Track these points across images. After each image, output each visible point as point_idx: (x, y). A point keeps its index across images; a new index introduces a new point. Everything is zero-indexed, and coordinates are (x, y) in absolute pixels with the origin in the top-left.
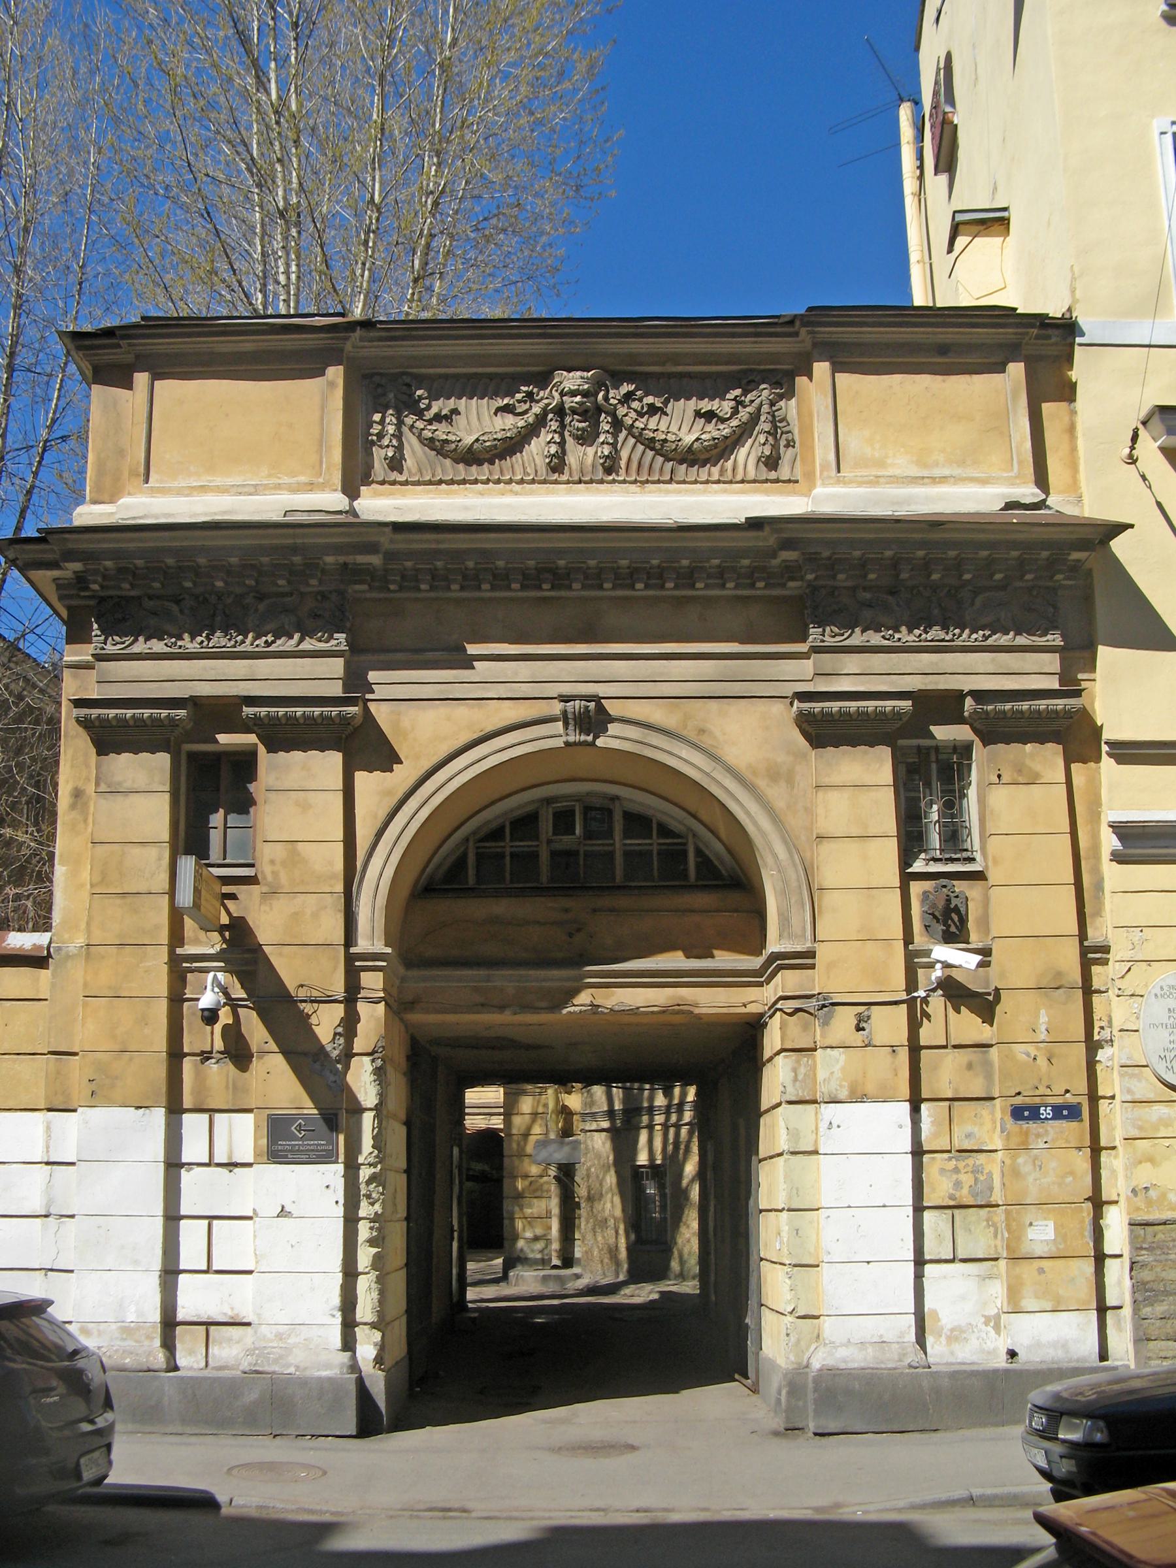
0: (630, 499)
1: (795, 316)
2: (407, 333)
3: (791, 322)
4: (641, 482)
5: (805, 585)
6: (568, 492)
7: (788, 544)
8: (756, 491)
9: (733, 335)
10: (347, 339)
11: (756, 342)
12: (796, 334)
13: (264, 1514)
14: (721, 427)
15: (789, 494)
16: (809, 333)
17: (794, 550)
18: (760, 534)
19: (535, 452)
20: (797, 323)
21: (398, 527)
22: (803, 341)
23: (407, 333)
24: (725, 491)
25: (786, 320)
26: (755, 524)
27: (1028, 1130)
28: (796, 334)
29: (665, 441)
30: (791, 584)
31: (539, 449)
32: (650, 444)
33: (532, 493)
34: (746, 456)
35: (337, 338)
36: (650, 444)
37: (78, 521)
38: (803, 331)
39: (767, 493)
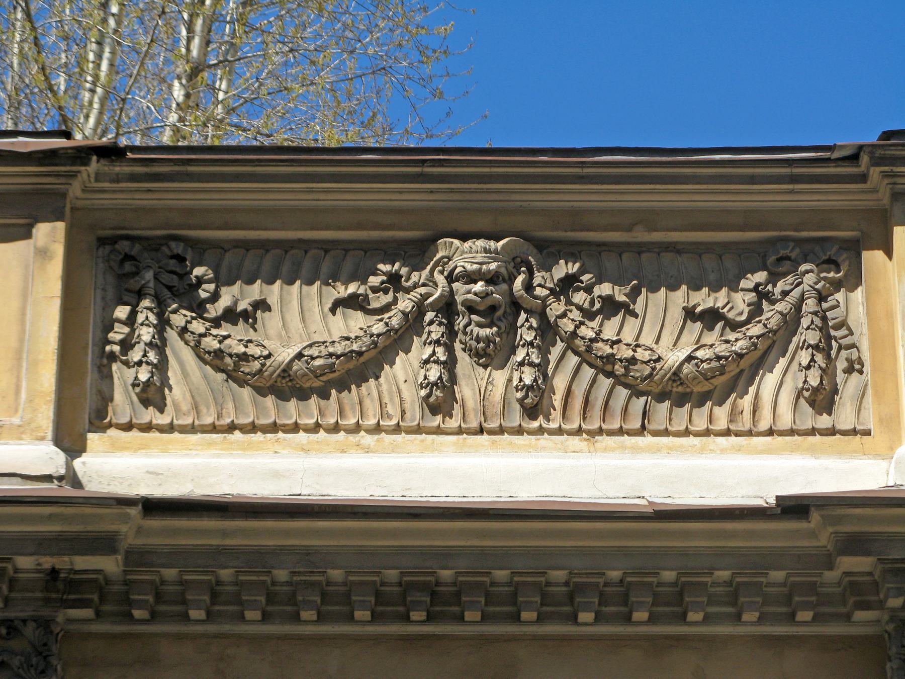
0: (570, 461)
1: (861, 147)
7: (854, 544)
8: (794, 450)
9: (752, 180)
10: (74, 175)
11: (792, 192)
12: (863, 178)
16: (886, 175)
17: (867, 553)
19: (401, 378)
20: (865, 159)
22: (875, 191)
24: (739, 449)
26: (794, 508)
28: (863, 178)
29: (633, 361)
32: (605, 366)
35: (57, 175)
36: (605, 366)
38: (875, 173)
39: (813, 451)
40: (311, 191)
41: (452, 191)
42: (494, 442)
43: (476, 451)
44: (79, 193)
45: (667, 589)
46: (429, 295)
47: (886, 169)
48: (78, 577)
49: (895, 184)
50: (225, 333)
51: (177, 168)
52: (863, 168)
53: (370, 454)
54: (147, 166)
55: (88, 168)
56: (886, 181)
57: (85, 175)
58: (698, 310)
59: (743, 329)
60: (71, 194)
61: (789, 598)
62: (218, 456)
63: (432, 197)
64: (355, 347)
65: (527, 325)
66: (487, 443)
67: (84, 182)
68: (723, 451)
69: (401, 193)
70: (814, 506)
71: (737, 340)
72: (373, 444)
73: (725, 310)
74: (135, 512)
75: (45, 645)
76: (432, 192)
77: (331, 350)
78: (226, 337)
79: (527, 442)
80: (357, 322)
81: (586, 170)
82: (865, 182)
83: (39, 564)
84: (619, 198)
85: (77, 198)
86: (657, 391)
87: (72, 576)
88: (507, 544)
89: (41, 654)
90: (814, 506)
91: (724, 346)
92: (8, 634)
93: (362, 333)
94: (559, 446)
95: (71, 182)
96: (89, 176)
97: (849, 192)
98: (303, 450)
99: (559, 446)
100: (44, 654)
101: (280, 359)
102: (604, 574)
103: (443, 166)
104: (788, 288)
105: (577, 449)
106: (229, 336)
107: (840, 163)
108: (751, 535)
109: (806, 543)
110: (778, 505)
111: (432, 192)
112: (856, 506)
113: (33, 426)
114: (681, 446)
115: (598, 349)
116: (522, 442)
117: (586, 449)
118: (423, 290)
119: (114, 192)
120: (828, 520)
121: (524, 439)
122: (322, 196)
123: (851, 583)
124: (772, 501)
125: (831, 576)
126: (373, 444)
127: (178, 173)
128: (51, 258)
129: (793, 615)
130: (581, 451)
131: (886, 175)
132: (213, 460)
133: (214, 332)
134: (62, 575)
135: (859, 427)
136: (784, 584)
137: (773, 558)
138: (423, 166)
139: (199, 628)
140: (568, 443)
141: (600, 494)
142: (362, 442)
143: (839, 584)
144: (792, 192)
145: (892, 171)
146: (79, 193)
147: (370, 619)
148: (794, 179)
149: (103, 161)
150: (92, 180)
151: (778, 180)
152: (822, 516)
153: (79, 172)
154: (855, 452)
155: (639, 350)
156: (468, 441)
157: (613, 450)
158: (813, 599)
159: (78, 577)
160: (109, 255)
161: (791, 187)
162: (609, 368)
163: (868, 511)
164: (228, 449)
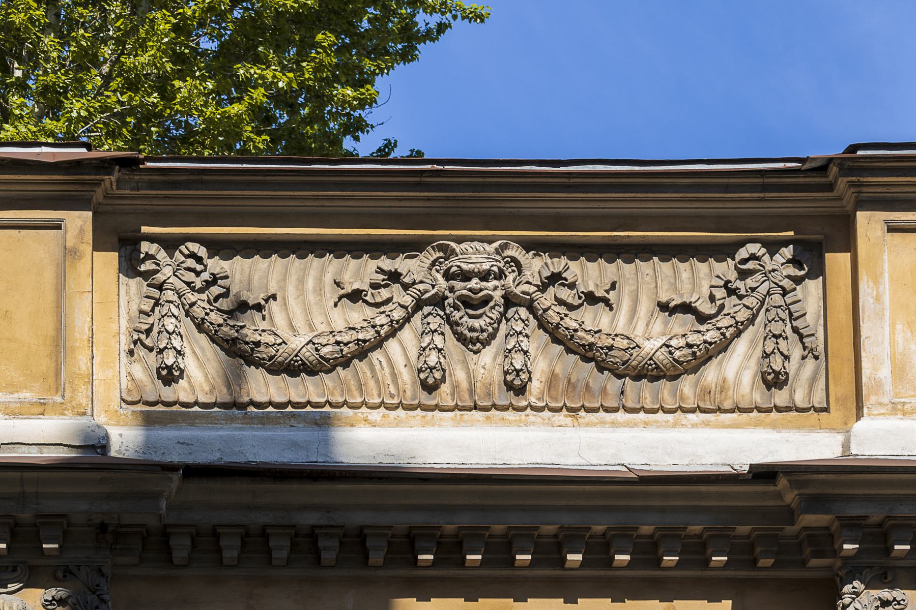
0: (557, 434)
1: (830, 160)
2: (197, 177)
3: (823, 167)
4: (570, 410)
5: (839, 563)
6: (457, 423)
7: (816, 503)
8: (757, 424)
9: (727, 188)
10: (98, 183)
11: (762, 200)
12: (830, 187)
13: (614, 242)
14: (703, 328)
15: (812, 428)
16: (852, 185)
17: (827, 513)
18: (771, 488)
20: (834, 170)
21: (195, 472)
22: (840, 198)
23: (197, 177)
24: (706, 424)
25: (814, 165)
26: (764, 474)
27: (414, 399)
28: (830, 187)
29: (611, 348)
30: (815, 562)
31: (401, 351)
32: (587, 353)
33: (398, 424)
34: (738, 368)
35: (82, 183)
36: (587, 353)
37: (737, 532)
38: (842, 182)
39: (774, 426)
40: (317, 198)
41: (447, 199)
42: (488, 418)
43: (472, 426)
44: (101, 199)
45: (497, 540)
46: (426, 291)
47: (854, 179)
48: (124, 530)
49: (860, 192)
50: (242, 324)
51: (192, 177)
52: (831, 178)
53: (377, 428)
54: (165, 175)
55: (111, 177)
56: (852, 190)
57: (107, 184)
58: (672, 304)
59: (714, 321)
60: (94, 200)
61: (752, 546)
62: (241, 429)
63: (428, 204)
64: (361, 336)
65: (516, 316)
66: (481, 419)
67: (106, 189)
68: (694, 426)
69: (400, 200)
70: (782, 472)
71: (708, 330)
72: (379, 419)
73: (697, 304)
74: (176, 477)
75: (98, 585)
76: (429, 199)
77: (339, 339)
78: (242, 327)
79: (518, 418)
80: (357, 314)
81: (572, 180)
82: (832, 191)
83: (90, 520)
84: (602, 205)
85: (99, 204)
86: (633, 374)
87: (119, 530)
88: (763, 504)
89: (94, 593)
90: (782, 472)
91: (696, 336)
92: (65, 576)
93: (365, 324)
94: (547, 421)
95: (95, 189)
96: (111, 184)
97: (816, 200)
98: (316, 424)
99: (547, 421)
100: (97, 593)
101: (293, 346)
102: (590, 528)
103: (440, 176)
104: (754, 285)
105: (562, 423)
106: (244, 326)
107: (809, 173)
108: (724, 496)
109: (771, 503)
110: (749, 472)
111: (429, 200)
112: (861, 473)
113: (74, 403)
114: (656, 422)
115: (581, 338)
116: (513, 418)
117: (570, 424)
118: (421, 287)
119: (133, 198)
120: (794, 484)
121: (510, 415)
122: (327, 203)
123: (809, 536)
124: (747, 468)
125: (789, 530)
126: (379, 419)
127: (193, 181)
128: (80, 258)
129: (755, 561)
130: (566, 426)
131: (852, 185)
132: (237, 433)
133: (231, 323)
134: (110, 529)
135: (702, 405)
136: (748, 537)
137: (743, 514)
138: (422, 176)
139: (382, 573)
140: (554, 419)
141: (583, 462)
142: (370, 417)
143: (797, 536)
144: (762, 200)
145: (859, 181)
146: (101, 199)
147: (333, 563)
148: (765, 188)
149: (124, 171)
150: (114, 188)
151: (751, 188)
152: (789, 481)
153: (103, 180)
154: (813, 427)
155: (618, 339)
156: (465, 417)
157: (595, 425)
158: (775, 549)
159: (124, 530)
160: (130, 255)
161: (762, 195)
162: (590, 355)
163: (831, 477)
164: (249, 423)
